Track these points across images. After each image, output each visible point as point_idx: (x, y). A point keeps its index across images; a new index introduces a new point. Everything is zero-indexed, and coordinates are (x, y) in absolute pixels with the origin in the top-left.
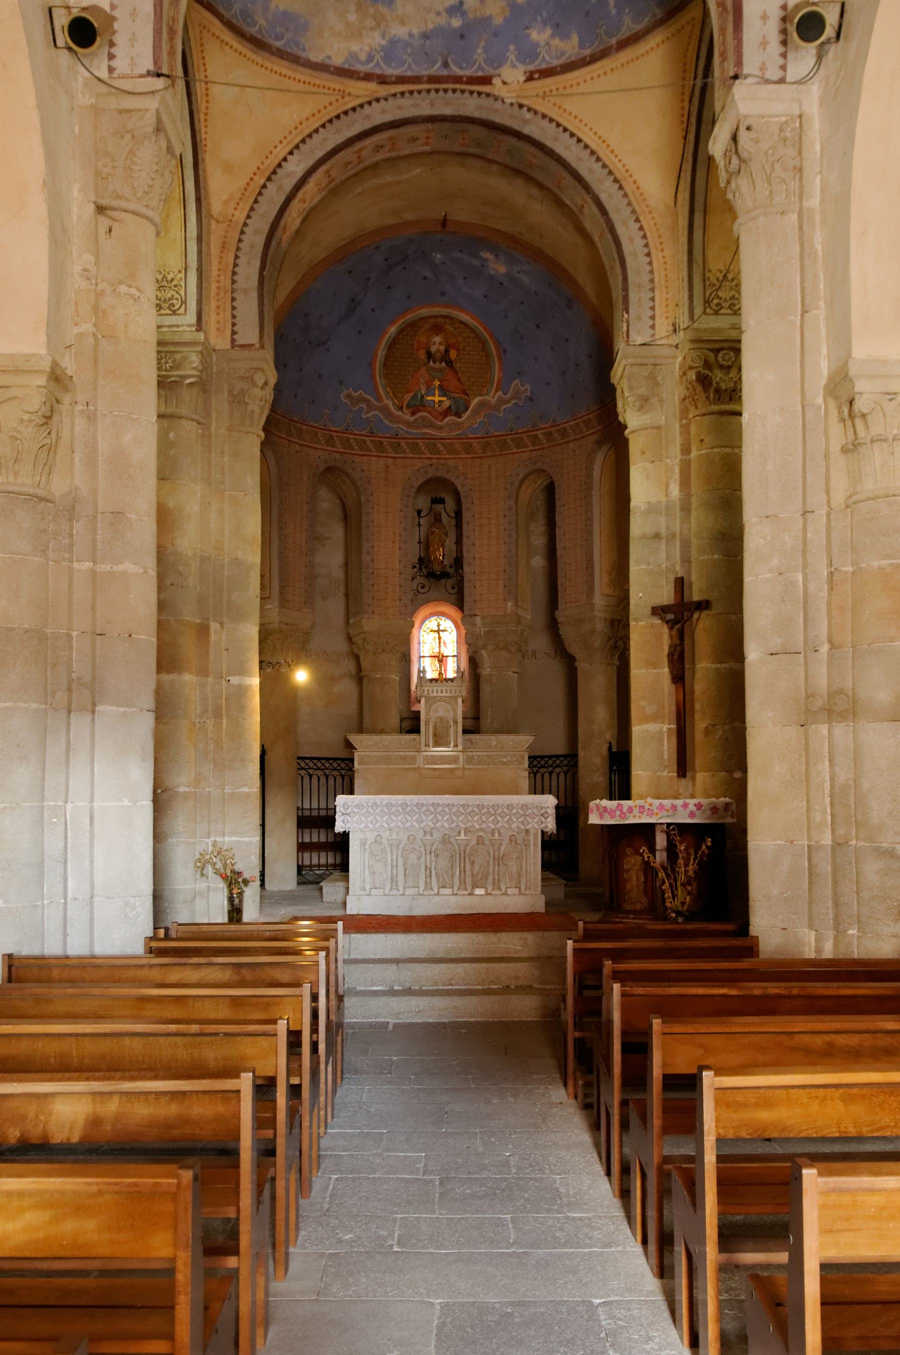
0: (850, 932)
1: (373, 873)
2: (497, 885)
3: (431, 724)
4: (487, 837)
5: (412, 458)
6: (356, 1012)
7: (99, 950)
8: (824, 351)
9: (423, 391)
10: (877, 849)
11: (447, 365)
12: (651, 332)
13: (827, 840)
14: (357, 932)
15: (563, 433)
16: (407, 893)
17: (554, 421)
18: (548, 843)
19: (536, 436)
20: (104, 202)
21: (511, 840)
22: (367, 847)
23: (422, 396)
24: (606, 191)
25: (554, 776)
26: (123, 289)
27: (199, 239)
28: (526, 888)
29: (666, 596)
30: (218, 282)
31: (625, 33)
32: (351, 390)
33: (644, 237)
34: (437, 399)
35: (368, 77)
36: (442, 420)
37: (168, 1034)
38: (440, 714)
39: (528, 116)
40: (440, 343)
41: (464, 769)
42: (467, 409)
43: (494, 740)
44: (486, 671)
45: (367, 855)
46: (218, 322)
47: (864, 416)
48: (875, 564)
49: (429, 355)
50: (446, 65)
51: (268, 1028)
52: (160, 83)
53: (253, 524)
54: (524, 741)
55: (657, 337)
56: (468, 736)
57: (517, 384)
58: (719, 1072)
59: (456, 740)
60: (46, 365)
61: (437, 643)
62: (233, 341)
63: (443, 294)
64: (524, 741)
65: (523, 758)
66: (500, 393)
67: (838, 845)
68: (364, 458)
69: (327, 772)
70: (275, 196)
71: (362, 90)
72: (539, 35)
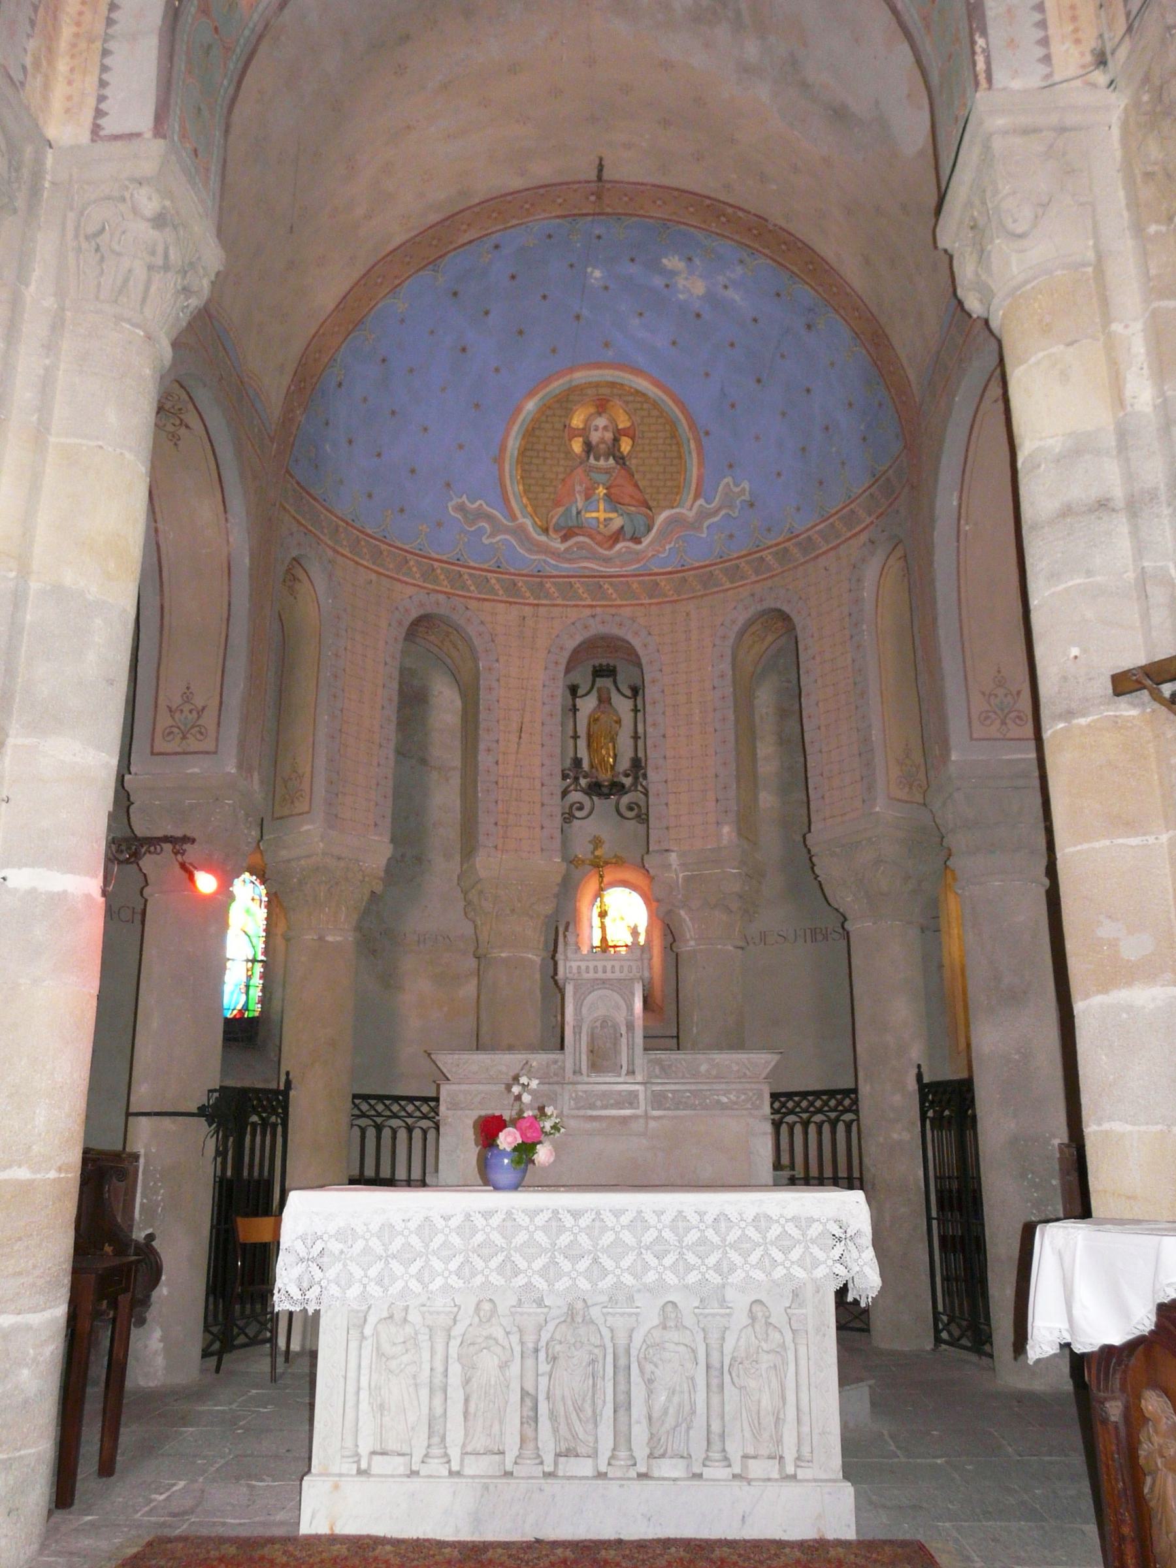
1: (382, 1407)
4: (688, 1304)
5: (564, 606)
9: (580, 505)
11: (617, 463)
12: (1042, 69)
15: (807, 546)
19: (762, 559)
21: (753, 1318)
22: (368, 1331)
23: (579, 513)
25: (812, 1129)
30: (78, 24)
32: (464, 498)
36: (611, 547)
38: (601, 1012)
40: (605, 428)
41: (646, 1116)
42: (649, 529)
43: (707, 1062)
44: (689, 943)
45: (366, 1352)
46: (69, 98)
49: (589, 447)
54: (763, 1060)
55: (1057, 78)
57: (728, 484)
59: (631, 1062)
61: (620, 915)
62: (96, 130)
63: (607, 345)
64: (763, 1060)
65: (760, 1096)
66: (701, 502)
68: (486, 603)
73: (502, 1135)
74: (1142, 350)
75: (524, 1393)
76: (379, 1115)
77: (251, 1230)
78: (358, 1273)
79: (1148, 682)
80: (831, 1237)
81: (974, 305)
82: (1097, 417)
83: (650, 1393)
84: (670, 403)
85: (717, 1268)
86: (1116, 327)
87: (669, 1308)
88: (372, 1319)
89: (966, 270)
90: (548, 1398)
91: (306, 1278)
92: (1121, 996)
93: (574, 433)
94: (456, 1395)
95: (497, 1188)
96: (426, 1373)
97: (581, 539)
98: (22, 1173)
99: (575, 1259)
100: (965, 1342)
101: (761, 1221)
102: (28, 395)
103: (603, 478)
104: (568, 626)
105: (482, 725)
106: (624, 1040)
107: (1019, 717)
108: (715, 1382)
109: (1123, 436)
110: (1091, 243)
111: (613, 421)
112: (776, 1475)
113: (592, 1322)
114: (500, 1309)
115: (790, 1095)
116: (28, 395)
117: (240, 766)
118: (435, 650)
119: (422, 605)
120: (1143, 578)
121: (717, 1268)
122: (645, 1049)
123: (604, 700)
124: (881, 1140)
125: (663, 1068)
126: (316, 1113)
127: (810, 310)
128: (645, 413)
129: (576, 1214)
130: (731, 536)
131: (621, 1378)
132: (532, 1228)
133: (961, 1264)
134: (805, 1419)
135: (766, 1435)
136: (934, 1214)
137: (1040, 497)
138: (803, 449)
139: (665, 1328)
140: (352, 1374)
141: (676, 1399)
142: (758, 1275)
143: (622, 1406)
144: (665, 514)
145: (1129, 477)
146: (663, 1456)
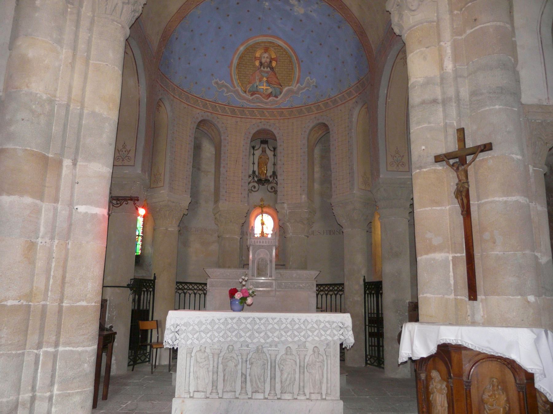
1: (197, 378)
3: (256, 262)
4: (294, 347)
9: (258, 83)
16: (224, 397)
17: (329, 96)
19: (319, 105)
21: (314, 352)
22: (193, 354)
23: (257, 86)
28: (327, 394)
29: (450, 145)
32: (218, 79)
38: (262, 256)
40: (267, 57)
41: (276, 291)
42: (281, 93)
43: (295, 273)
44: (290, 234)
49: (261, 64)
54: (314, 273)
56: (278, 271)
59: (271, 273)
61: (264, 225)
63: (269, 29)
64: (314, 273)
66: (299, 84)
69: (195, 291)
73: (236, 294)
74: (450, 52)
75: (242, 374)
76: (185, 289)
77: (143, 325)
78: (191, 336)
79: (445, 159)
80: (339, 327)
81: (397, 31)
82: (434, 72)
83: (282, 374)
84: (291, 51)
85: (304, 336)
86: (442, 43)
87: (288, 349)
88: (194, 351)
89: (395, 19)
90: (250, 375)
91: (174, 338)
92: (432, 256)
93: (256, 58)
94: (221, 374)
95: (234, 311)
96: (211, 367)
97: (257, 95)
98: (84, 303)
99: (259, 333)
100: (375, 364)
101: (318, 322)
102: (83, 46)
103: (266, 75)
104: (253, 125)
105: (222, 158)
106: (269, 266)
107: (403, 164)
108: (302, 371)
109: (443, 79)
110: (436, 15)
111: (270, 55)
112: (319, 398)
113: (264, 352)
114: (235, 348)
116: (83, 46)
117: (142, 171)
118: (206, 132)
119: (202, 116)
120: (446, 125)
121: (304, 336)
122: (276, 269)
123: (264, 151)
124: (351, 300)
125: (281, 275)
126: (164, 287)
127: (340, 22)
128: (281, 53)
129: (260, 319)
130: (309, 97)
131: (273, 369)
132: (246, 323)
133: (375, 335)
134: (329, 382)
135: (317, 387)
136: (367, 324)
137: (415, 97)
138: (335, 69)
139: (287, 354)
140: (188, 368)
141: (290, 376)
142: (317, 338)
143: (273, 378)
145: (443, 93)
146: (285, 393)
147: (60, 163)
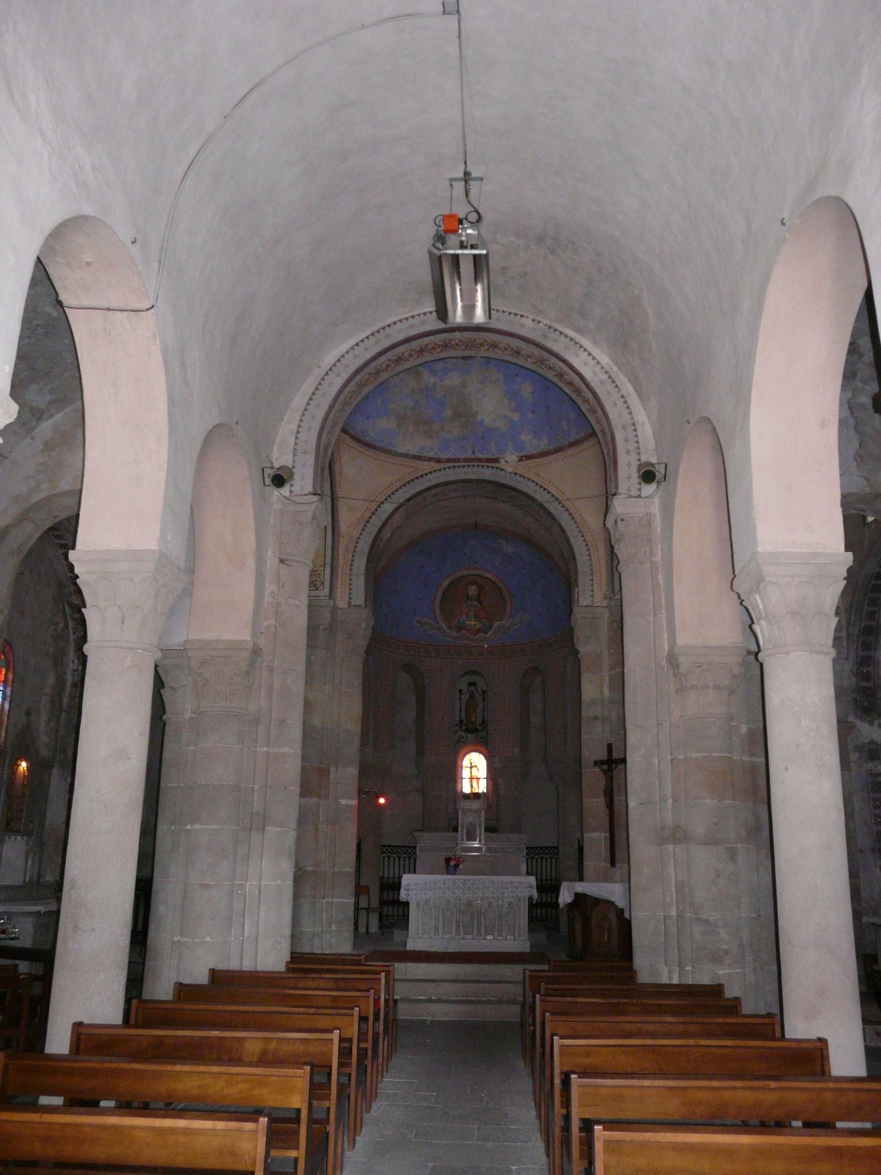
0: (688, 968)
2: (500, 933)
6: (404, 1012)
7: (259, 968)
8: (666, 637)
9: (464, 617)
10: (698, 919)
13: (674, 913)
14: (411, 962)
18: (533, 905)
20: (284, 557)
24: (565, 521)
26: (291, 601)
27: (333, 549)
29: (603, 755)
31: (572, 440)
33: (587, 545)
34: (472, 623)
35: (430, 459)
37: (299, 1014)
38: (470, 820)
39: (520, 479)
42: (491, 629)
47: (685, 675)
48: (694, 755)
50: (474, 452)
51: (349, 1011)
52: (316, 498)
53: (357, 708)
58: (562, 1038)
60: (250, 646)
61: (474, 771)
62: (349, 603)
67: (680, 916)
70: (376, 523)
71: (426, 466)
72: (525, 437)
80: (524, 886)
115: (532, 848)
133: (549, 887)
143: (479, 924)
144: (497, 623)
147: (329, 771)
